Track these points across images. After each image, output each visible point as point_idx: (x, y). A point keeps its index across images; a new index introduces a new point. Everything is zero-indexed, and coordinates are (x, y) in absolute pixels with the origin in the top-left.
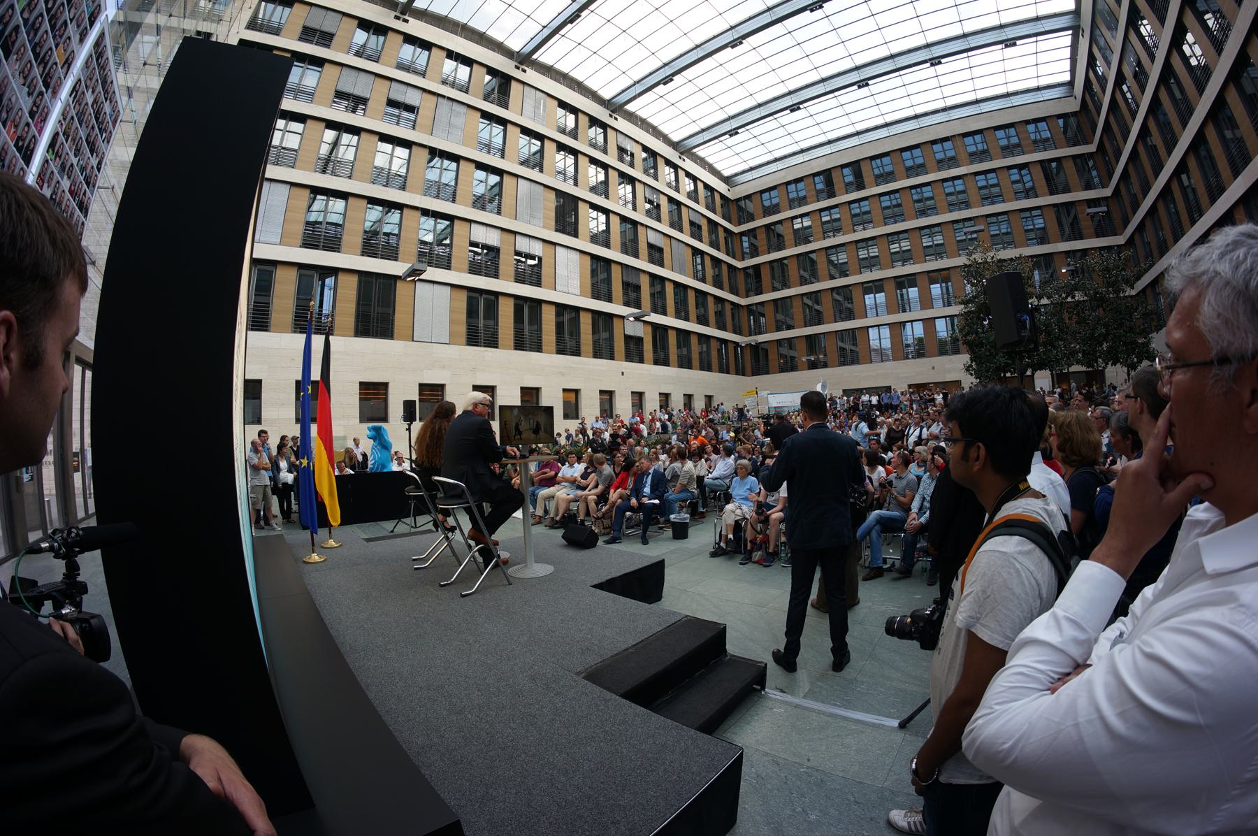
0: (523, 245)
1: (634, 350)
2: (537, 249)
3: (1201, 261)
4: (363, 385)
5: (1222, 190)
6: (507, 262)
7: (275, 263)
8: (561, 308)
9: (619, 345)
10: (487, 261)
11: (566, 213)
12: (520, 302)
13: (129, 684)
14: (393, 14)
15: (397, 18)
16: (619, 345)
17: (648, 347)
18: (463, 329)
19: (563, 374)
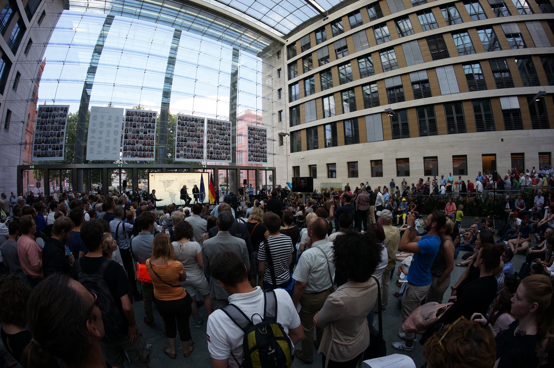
0: (414, 78)
1: (512, 120)
2: (423, 76)
3: (553, 237)
4: (348, 163)
5: (296, 55)
6: (408, 90)
7: (316, 126)
8: (447, 105)
9: (499, 119)
10: (395, 94)
11: (437, 46)
12: (545, 59)
13: (122, 264)
14: (322, 20)
15: (324, 20)
16: (499, 119)
17: (526, 116)
18: (390, 132)
19: (452, 146)
